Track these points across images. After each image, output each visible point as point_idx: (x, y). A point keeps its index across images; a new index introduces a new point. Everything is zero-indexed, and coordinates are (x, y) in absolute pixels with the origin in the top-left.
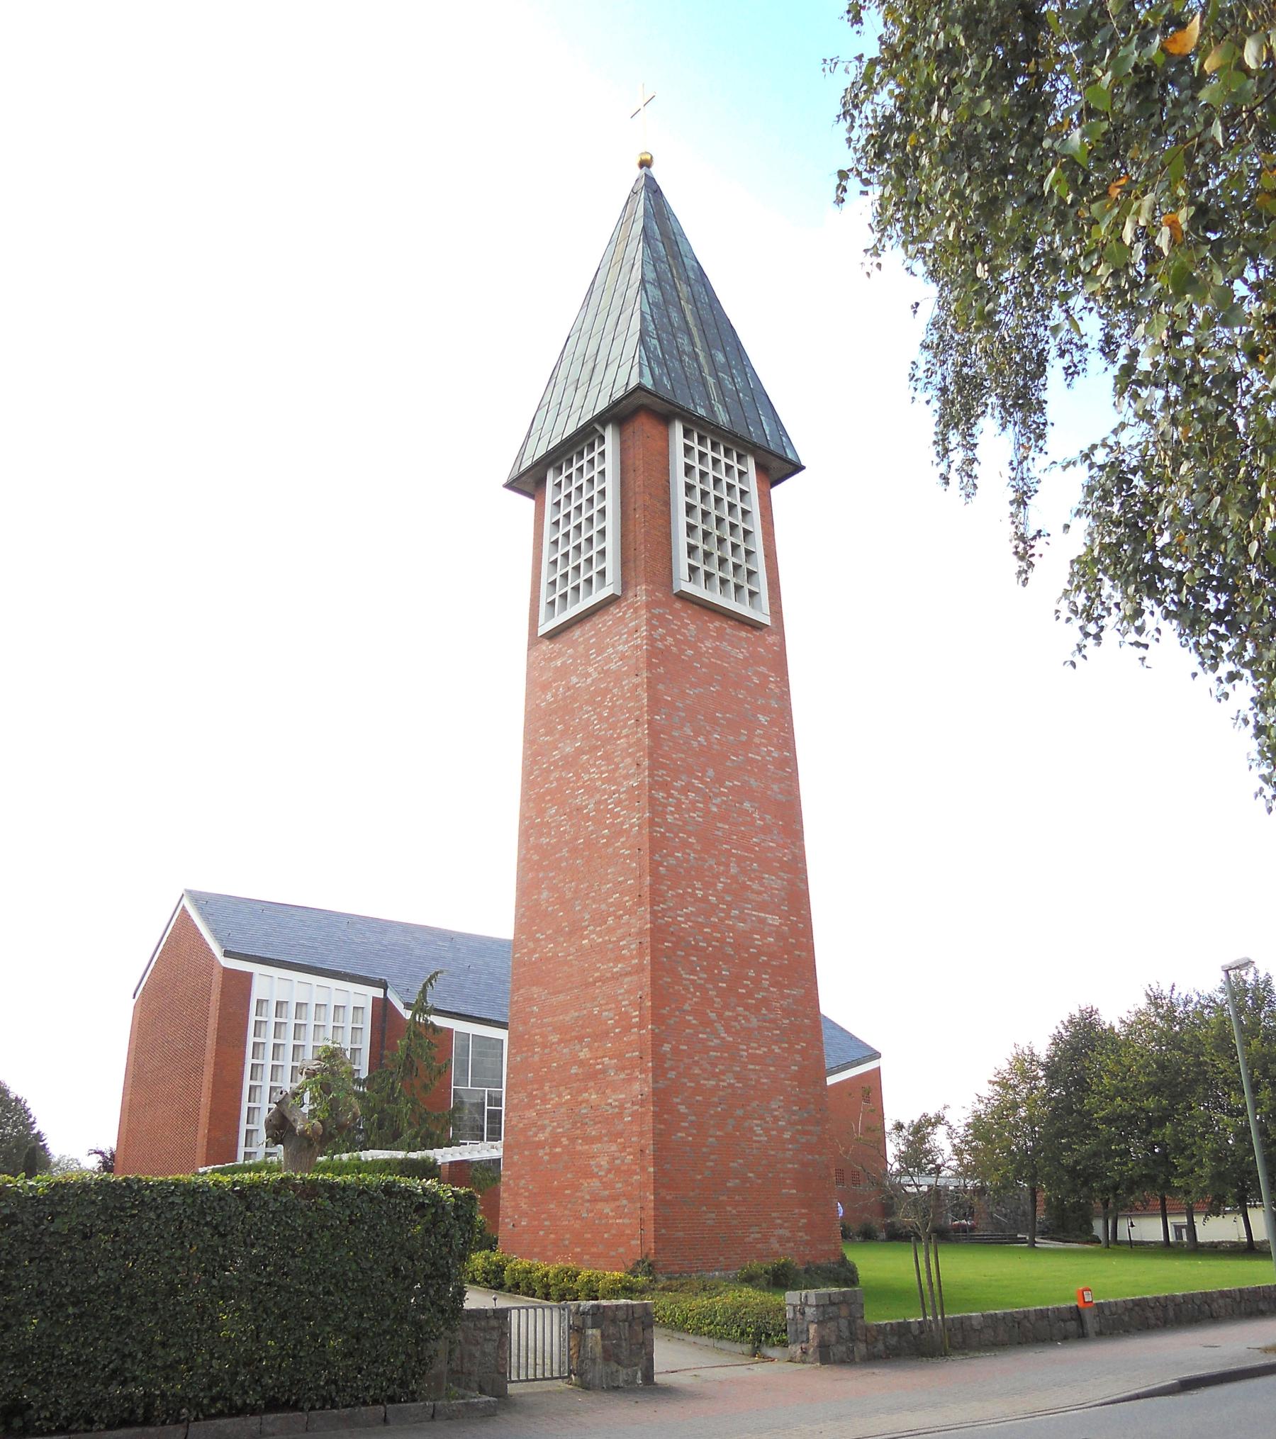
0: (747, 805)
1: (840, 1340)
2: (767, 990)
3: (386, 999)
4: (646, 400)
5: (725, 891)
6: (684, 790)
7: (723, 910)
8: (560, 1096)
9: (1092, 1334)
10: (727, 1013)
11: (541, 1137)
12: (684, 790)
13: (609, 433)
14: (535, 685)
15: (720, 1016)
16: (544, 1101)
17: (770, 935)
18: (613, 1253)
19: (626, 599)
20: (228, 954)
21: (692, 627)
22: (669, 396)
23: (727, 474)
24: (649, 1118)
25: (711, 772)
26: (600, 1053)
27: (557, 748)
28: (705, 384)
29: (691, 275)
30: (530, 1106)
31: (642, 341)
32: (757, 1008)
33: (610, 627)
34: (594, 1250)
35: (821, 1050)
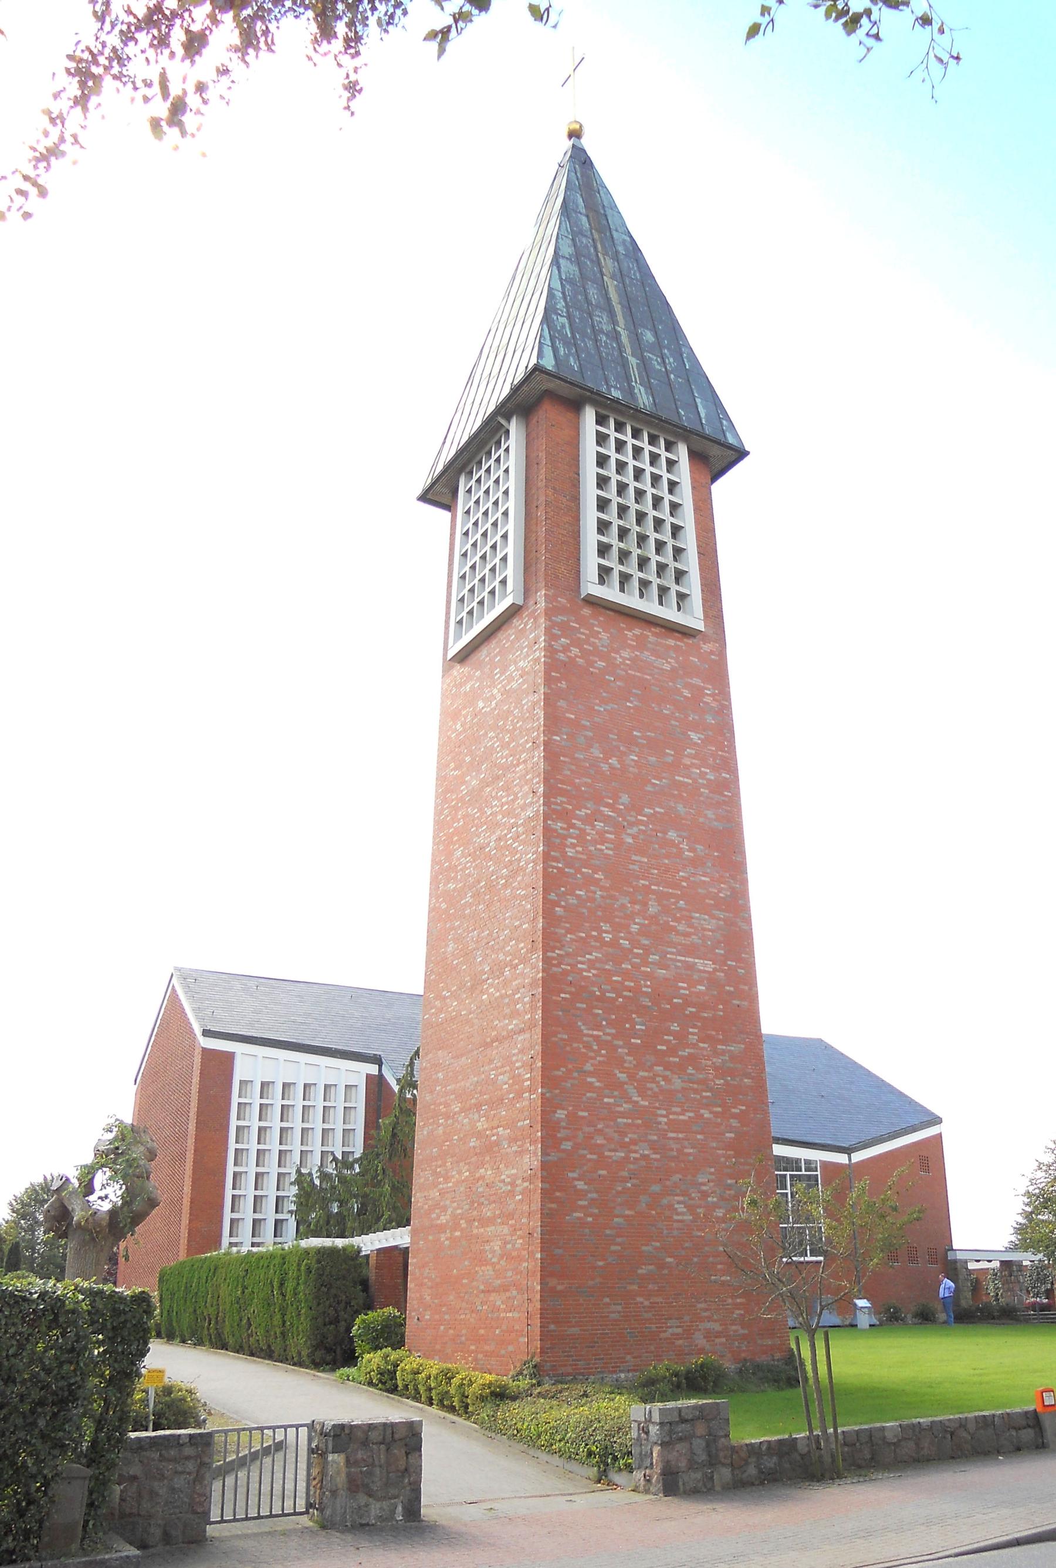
0: (672, 835)
1: (692, 1465)
2: (694, 1046)
3: (381, 1076)
4: (552, 385)
5: (640, 933)
6: (589, 820)
7: (637, 955)
8: (460, 1173)
9: (718, 1488)
10: (642, 1074)
11: (443, 1219)
12: (589, 820)
13: (514, 427)
14: (449, 715)
15: (632, 1077)
16: (447, 1179)
17: (700, 982)
18: (503, 1352)
19: (527, 608)
20: (206, 1033)
21: (604, 636)
22: (578, 379)
23: (652, 464)
24: (537, 1197)
25: (625, 798)
26: (495, 1123)
27: (464, 782)
28: (625, 363)
29: (621, 249)
30: (435, 1185)
31: (547, 319)
32: (680, 1068)
33: (512, 642)
34: (487, 1348)
35: (766, 1113)
